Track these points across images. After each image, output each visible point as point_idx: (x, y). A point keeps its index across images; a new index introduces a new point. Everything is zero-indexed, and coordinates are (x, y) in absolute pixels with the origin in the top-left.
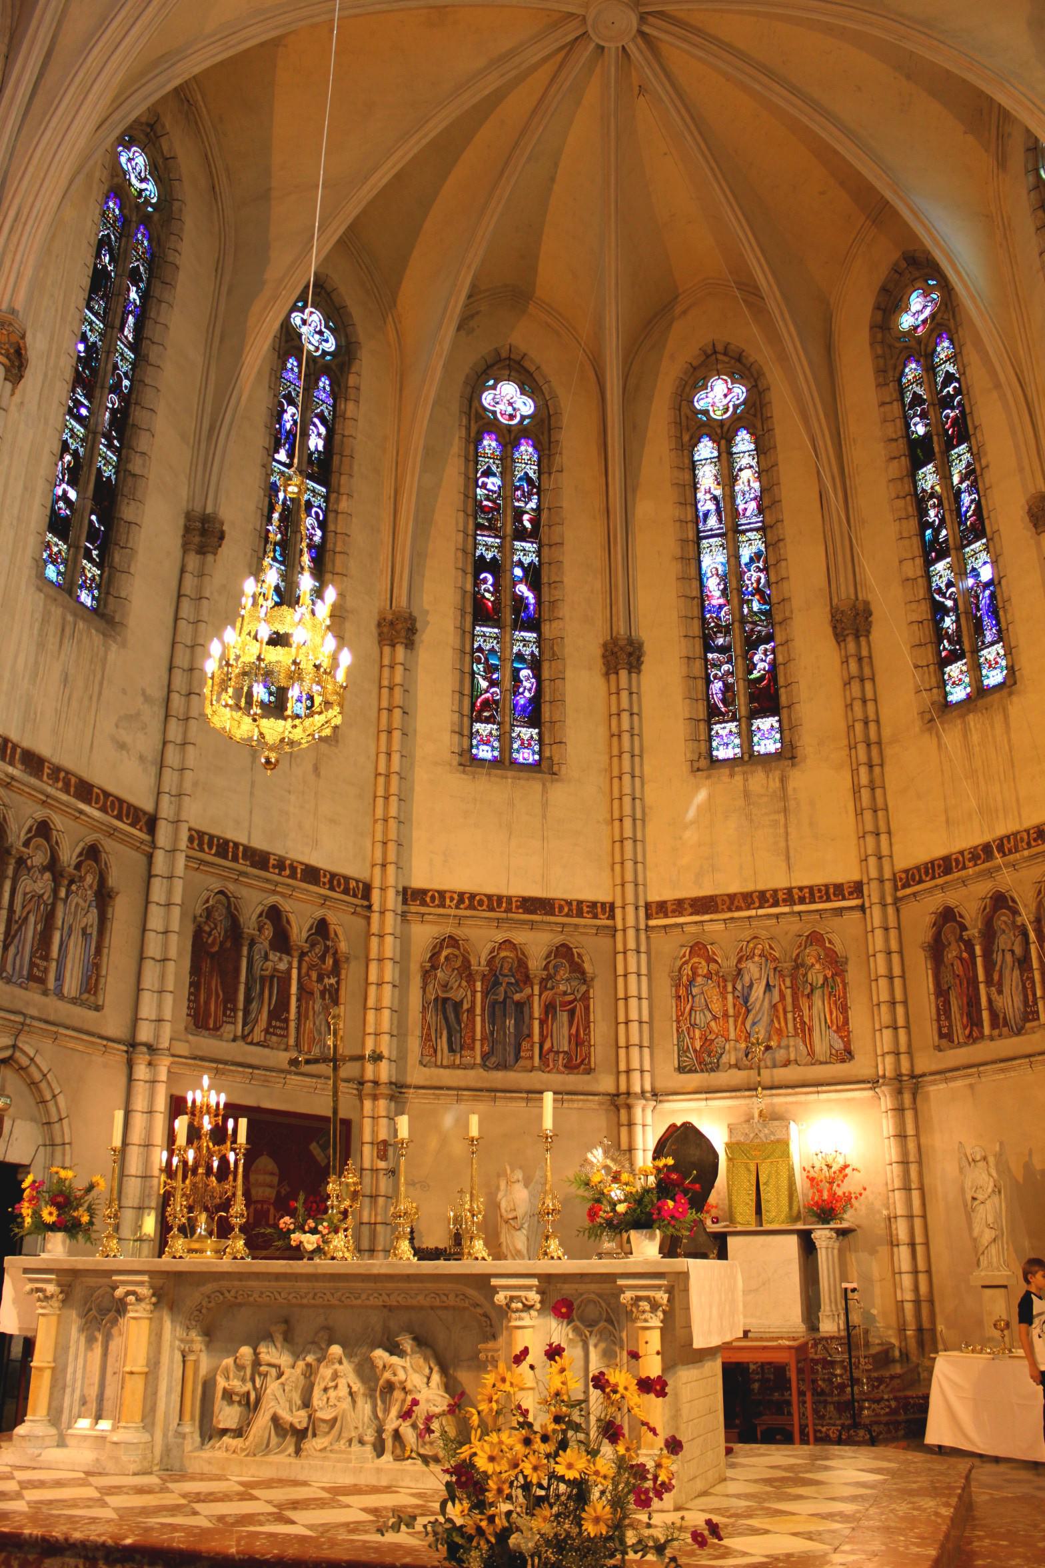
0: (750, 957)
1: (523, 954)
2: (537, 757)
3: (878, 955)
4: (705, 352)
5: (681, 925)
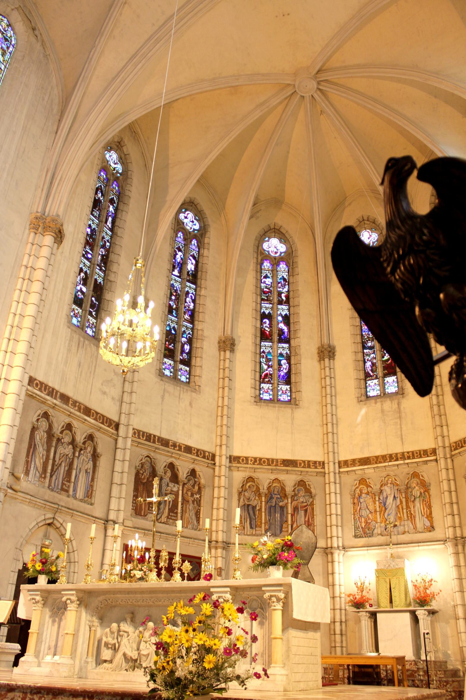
0: (386, 484)
1: (284, 485)
2: (289, 398)
3: (444, 481)
4: (359, 220)
5: (354, 471)
